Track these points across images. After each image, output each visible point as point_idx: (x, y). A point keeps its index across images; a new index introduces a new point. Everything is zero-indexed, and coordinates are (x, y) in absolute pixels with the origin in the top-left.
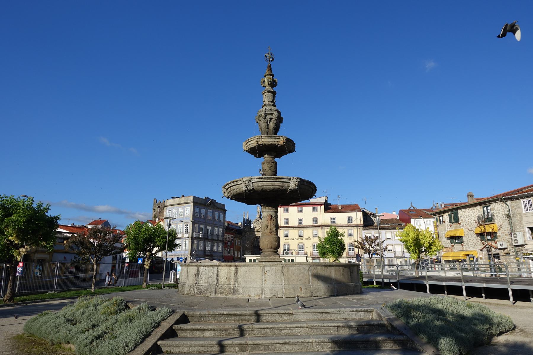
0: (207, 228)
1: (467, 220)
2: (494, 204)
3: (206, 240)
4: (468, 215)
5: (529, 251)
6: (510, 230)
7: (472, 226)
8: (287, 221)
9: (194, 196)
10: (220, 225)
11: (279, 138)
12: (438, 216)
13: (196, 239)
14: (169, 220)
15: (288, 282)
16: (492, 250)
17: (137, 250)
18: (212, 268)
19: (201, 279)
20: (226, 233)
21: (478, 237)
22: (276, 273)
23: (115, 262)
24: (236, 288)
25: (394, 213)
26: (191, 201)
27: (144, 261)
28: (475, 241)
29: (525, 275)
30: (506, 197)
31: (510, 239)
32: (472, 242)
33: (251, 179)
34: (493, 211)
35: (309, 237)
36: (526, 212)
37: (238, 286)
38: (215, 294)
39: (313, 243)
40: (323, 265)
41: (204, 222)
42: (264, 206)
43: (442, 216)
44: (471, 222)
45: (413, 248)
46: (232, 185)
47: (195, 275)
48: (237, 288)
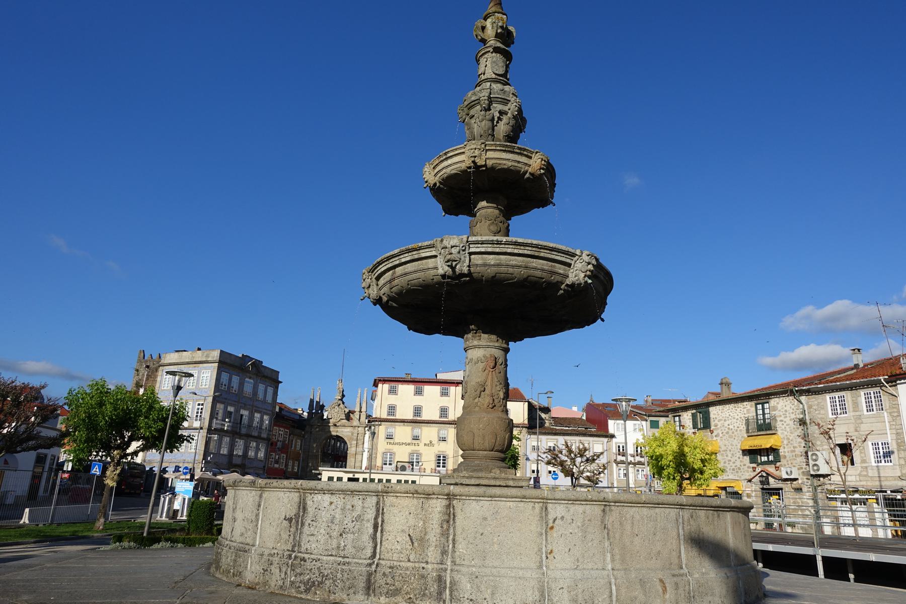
0: (241, 413)
1: (726, 425)
2: (777, 399)
3: (236, 436)
4: (727, 415)
5: (837, 486)
6: (804, 447)
7: (734, 437)
8: (394, 410)
9: (221, 351)
10: (265, 409)
11: (529, 154)
12: (672, 415)
13: (217, 433)
14: (177, 378)
15: (623, 561)
16: (770, 481)
17: (91, 443)
18: (357, 501)
19: (312, 535)
20: (275, 425)
21: (745, 457)
22: (584, 529)
23: (39, 470)
24: (448, 576)
25: (575, 409)
26: (213, 358)
27: (104, 470)
28: (738, 463)
29: (828, 530)
30: (802, 388)
31: (803, 462)
32: (734, 465)
33: (467, 242)
34: (774, 413)
35: (431, 442)
36: (869, 413)
37: (456, 568)
38: (368, 594)
39: (437, 452)
40: (712, 507)
41: (235, 401)
42: (477, 330)
43: (679, 416)
44: (733, 430)
45: (671, 470)
46: (403, 260)
47: (290, 520)
48: (452, 577)
